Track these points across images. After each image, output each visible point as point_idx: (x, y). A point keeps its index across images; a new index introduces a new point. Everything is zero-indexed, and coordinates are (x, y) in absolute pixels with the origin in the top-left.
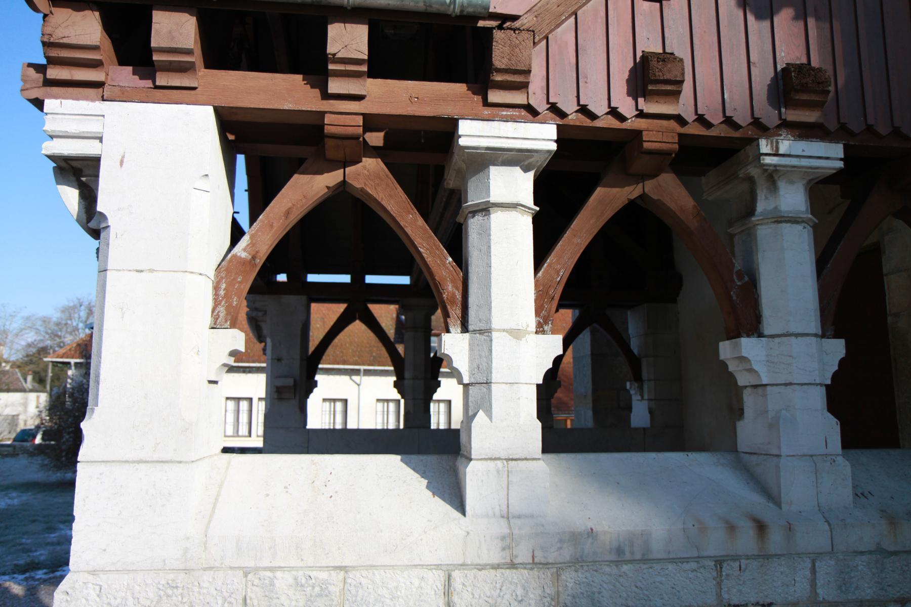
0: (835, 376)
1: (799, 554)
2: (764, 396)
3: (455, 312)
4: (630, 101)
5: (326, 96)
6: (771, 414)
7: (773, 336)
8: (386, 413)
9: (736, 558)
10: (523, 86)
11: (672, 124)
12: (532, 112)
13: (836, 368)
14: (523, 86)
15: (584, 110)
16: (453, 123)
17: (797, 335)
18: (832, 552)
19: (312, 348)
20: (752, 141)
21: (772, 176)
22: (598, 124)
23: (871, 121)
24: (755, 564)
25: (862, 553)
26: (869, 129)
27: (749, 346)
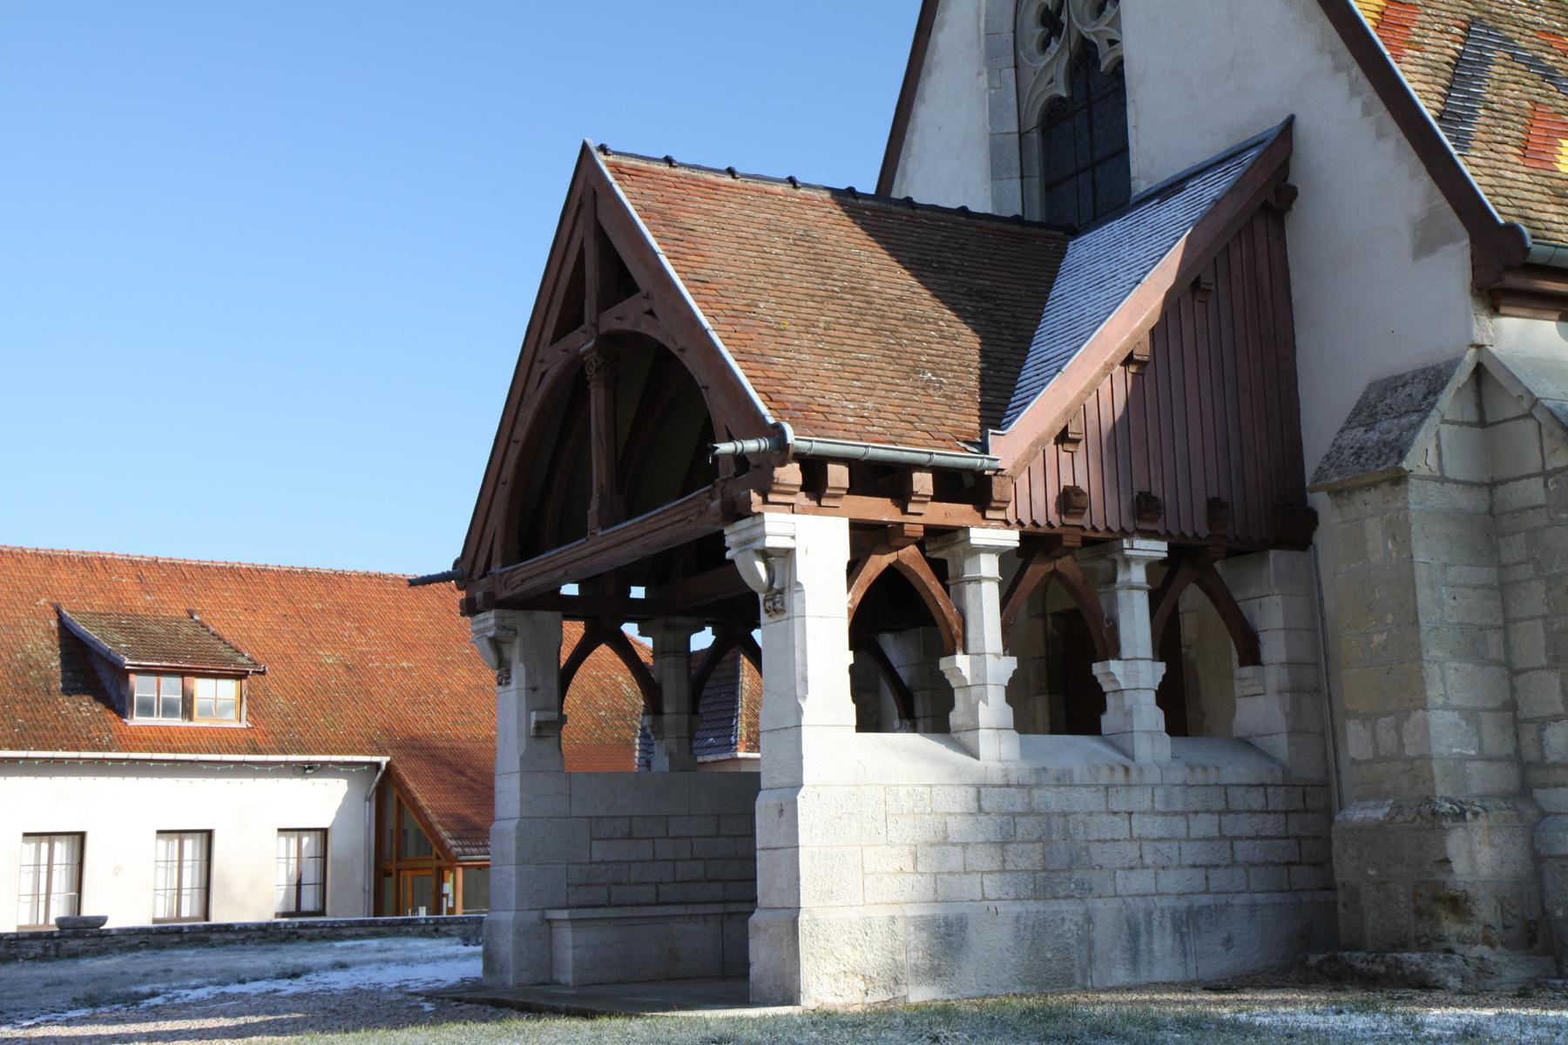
0: (1161, 685)
1: (1146, 785)
2: (1122, 696)
3: (959, 642)
4: (1057, 517)
5: (905, 511)
6: (1127, 707)
7: (1127, 660)
8: (44, 869)
9: (1115, 786)
10: (1004, 509)
11: (1078, 530)
12: (1007, 523)
13: (1160, 680)
14: (1004, 509)
15: (1034, 523)
16: (966, 529)
17: (1141, 659)
18: (1162, 784)
20: (1119, 540)
22: (1040, 530)
23: (1182, 529)
24: (1124, 789)
25: (1177, 785)
26: (1182, 533)
27: (1114, 666)
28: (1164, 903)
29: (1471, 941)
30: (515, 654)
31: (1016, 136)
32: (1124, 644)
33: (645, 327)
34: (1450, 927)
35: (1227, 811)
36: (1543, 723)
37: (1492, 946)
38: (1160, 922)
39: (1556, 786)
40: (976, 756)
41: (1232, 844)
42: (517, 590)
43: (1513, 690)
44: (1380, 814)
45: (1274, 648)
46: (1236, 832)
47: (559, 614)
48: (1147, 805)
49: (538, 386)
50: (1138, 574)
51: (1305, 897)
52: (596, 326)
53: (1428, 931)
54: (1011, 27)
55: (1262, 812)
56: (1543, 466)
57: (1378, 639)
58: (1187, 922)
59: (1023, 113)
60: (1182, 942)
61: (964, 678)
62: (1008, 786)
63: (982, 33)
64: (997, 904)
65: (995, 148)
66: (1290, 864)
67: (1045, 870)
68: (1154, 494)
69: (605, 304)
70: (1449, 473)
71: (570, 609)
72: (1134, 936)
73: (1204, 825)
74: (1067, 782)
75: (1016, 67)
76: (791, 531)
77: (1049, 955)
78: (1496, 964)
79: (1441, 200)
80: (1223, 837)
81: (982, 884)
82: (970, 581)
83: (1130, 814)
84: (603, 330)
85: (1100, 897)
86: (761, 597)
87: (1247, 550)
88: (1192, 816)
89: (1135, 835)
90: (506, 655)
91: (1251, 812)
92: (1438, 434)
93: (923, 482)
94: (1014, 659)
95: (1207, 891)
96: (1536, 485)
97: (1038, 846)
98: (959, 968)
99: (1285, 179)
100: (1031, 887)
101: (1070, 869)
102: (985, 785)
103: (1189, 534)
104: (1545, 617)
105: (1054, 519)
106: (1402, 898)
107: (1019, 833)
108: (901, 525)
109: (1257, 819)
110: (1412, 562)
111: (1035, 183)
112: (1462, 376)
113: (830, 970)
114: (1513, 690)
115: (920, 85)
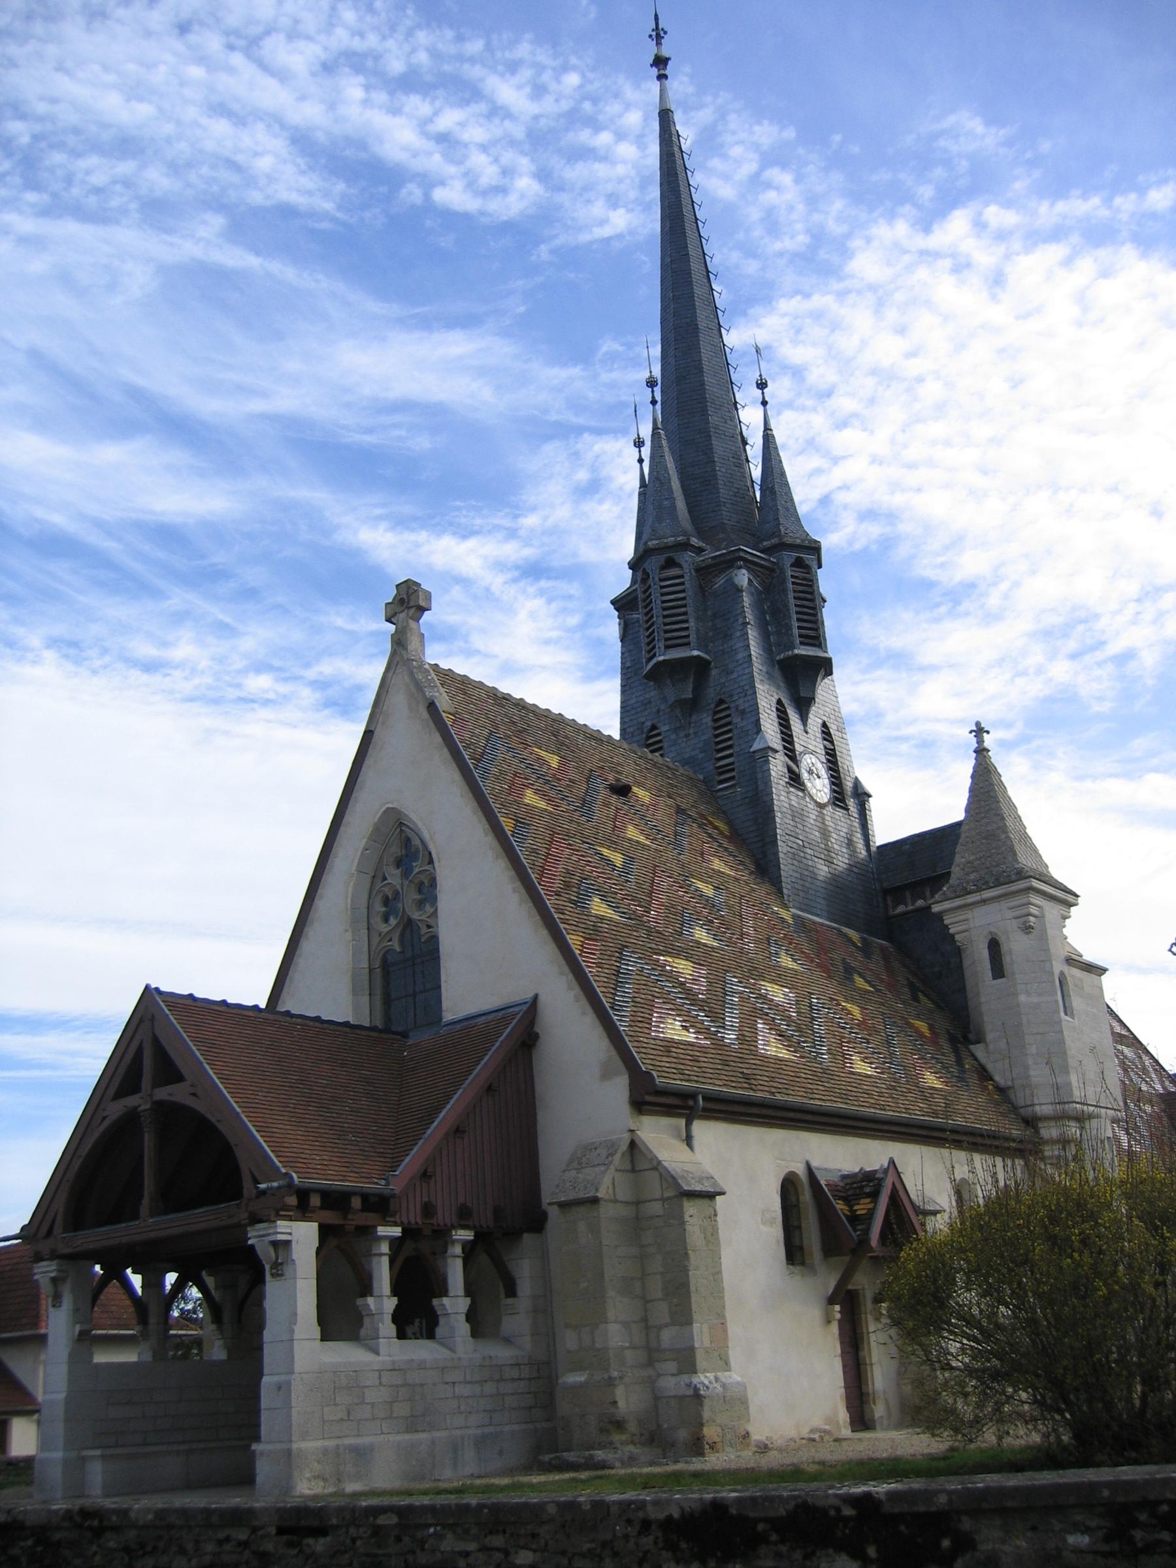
5: (345, 1218)
20: (451, 1231)
27: (445, 1300)
28: (470, 1432)
29: (626, 1443)
31: (368, 970)
33: (190, 1102)
34: (617, 1437)
35: (501, 1380)
36: (659, 1328)
39: (665, 1361)
40: (377, 1353)
42: (78, 1249)
44: (582, 1379)
45: (525, 1287)
49: (100, 1124)
51: (538, 1425)
52: (151, 1095)
54: (366, 906)
55: (518, 1379)
56: (662, 1195)
57: (584, 1285)
58: (481, 1442)
59: (372, 957)
61: (371, 1310)
62: (395, 1370)
63: (349, 907)
66: (531, 1408)
68: (469, 1204)
73: (489, 1388)
75: (368, 929)
77: (414, 1463)
79: (614, 1053)
82: (376, 1255)
85: (439, 1430)
86: (267, 1267)
87: (513, 1235)
91: (513, 1380)
92: (613, 1179)
93: (356, 1203)
95: (490, 1425)
99: (533, 1028)
102: (383, 1370)
103: (485, 1226)
105: (419, 1221)
108: (343, 1225)
112: (624, 1146)
113: (308, 1475)
114: (646, 1310)
115: (305, 929)
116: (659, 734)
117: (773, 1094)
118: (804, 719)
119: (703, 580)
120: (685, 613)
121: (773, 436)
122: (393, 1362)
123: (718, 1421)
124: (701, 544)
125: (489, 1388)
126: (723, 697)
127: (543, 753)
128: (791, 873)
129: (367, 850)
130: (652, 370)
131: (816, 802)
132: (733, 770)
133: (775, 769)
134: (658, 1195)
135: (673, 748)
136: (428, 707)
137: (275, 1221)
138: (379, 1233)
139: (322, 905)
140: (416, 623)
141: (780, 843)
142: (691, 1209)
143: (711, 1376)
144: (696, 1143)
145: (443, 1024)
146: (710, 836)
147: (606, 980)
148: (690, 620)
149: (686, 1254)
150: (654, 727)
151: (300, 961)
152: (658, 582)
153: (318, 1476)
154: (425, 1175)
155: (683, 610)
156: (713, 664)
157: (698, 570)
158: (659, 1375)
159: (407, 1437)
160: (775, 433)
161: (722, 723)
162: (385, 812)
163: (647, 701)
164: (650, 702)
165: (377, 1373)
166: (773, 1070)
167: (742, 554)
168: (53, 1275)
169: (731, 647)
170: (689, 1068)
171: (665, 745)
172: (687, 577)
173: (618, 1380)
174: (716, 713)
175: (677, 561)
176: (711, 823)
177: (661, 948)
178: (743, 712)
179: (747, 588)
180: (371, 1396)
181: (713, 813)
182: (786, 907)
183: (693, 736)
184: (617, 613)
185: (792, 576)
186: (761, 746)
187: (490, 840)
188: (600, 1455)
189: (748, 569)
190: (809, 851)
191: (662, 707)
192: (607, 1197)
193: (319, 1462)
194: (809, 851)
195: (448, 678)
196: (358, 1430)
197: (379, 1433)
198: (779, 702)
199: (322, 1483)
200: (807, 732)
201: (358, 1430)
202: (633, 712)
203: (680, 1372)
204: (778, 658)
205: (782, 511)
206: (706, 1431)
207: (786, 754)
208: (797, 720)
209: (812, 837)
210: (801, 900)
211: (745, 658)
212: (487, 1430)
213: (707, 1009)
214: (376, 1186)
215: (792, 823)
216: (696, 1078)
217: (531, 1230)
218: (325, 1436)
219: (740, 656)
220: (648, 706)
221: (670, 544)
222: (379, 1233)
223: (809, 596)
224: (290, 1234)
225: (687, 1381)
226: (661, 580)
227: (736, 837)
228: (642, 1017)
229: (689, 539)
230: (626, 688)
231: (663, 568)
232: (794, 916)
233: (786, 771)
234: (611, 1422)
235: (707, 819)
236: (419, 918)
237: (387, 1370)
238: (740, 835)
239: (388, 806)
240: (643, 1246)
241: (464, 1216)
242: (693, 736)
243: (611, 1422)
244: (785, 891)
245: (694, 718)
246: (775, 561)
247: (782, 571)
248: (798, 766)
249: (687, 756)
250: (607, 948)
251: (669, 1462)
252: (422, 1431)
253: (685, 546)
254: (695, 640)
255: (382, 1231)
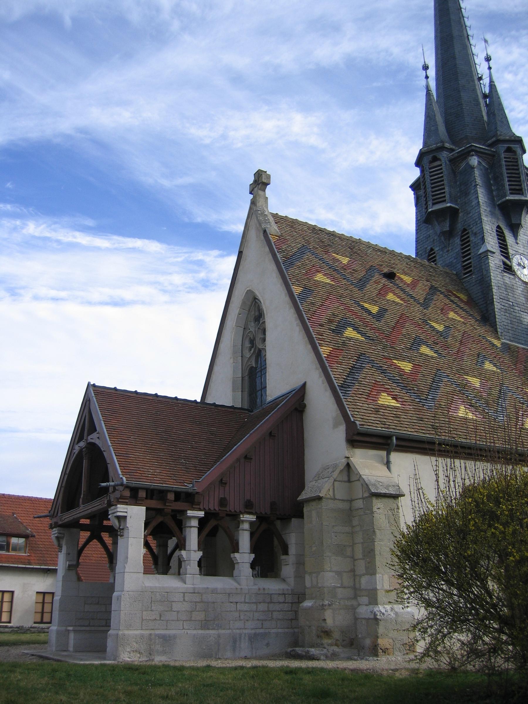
5: (165, 505)
10: (199, 505)
19: (80, 546)
21: (243, 521)
22: (212, 512)
27: (236, 555)
29: (331, 645)
30: (64, 543)
32: (240, 548)
34: (326, 641)
35: (271, 602)
36: (360, 576)
37: (338, 646)
38: (244, 638)
39: (363, 596)
41: (272, 613)
42: (63, 522)
43: (354, 566)
45: (292, 550)
46: (274, 609)
47: (79, 530)
48: (243, 600)
50: (246, 526)
52: (87, 440)
53: (319, 642)
55: (283, 603)
57: (314, 549)
58: (253, 638)
60: (251, 644)
64: (188, 631)
65: (234, 382)
66: (292, 619)
67: (205, 620)
68: (252, 500)
69: (90, 433)
70: (337, 497)
71: (84, 528)
72: (235, 641)
73: (262, 607)
74: (215, 592)
75: (242, 356)
76: (126, 511)
77: (204, 648)
78: (338, 652)
80: (269, 611)
81: (183, 624)
83: (237, 603)
84: (88, 441)
85: (224, 629)
87: (286, 519)
88: (258, 604)
89: (238, 610)
90: (61, 543)
91: (280, 603)
93: (171, 496)
94: (202, 552)
95: (262, 628)
96: (361, 501)
97: (204, 613)
98: (173, 651)
99: (303, 401)
100: (200, 625)
101: (214, 620)
102: (186, 593)
104: (362, 543)
106: (314, 631)
107: (197, 608)
109: (281, 605)
110: (322, 525)
111: (246, 394)
112: (342, 467)
113: (128, 650)
116: (434, 253)
117: (454, 438)
118: (515, 236)
119: (454, 166)
120: (443, 185)
121: (495, 85)
122: (194, 588)
123: (390, 635)
124: (452, 147)
125: (262, 607)
126: (465, 227)
127: (338, 257)
128: (504, 320)
129: (240, 314)
130: (426, 61)
131: (523, 281)
132: (471, 267)
133: (493, 262)
134: (361, 496)
135: (441, 259)
136: (264, 233)
137: (116, 505)
138: (188, 515)
139: (222, 346)
140: (263, 192)
141: (495, 303)
142: (378, 505)
143: (388, 607)
144: (392, 466)
145: (267, 403)
146: (452, 301)
147: (342, 371)
148: (446, 188)
149: (374, 531)
150: (432, 249)
151: (214, 377)
152: (428, 170)
153: (136, 651)
154: (222, 482)
155: (442, 183)
156: (460, 210)
157: (450, 161)
158: (359, 605)
159: (200, 632)
160: (496, 84)
161: (465, 242)
162: (246, 293)
163: (428, 236)
164: (430, 236)
165: (182, 594)
166: (458, 425)
167: (473, 148)
168: (56, 535)
169: (469, 199)
170: (390, 421)
171: (437, 258)
172: (443, 165)
173: (327, 607)
174: (462, 236)
175: (438, 157)
176: (455, 295)
177: (392, 356)
178: (475, 234)
179: (477, 166)
180: (176, 607)
181: (458, 291)
182: (498, 339)
183: (451, 251)
184: (413, 192)
185: (505, 158)
186: (484, 250)
187: (287, 299)
188: (313, 651)
189: (479, 157)
190: (517, 308)
191: (436, 238)
192: (328, 496)
193: (137, 643)
194: (517, 308)
195: (279, 219)
196: (167, 626)
197: (182, 628)
198: (498, 227)
199: (139, 655)
200: (517, 243)
201: (167, 626)
202: (421, 243)
203: (370, 604)
204: (498, 203)
205: (499, 123)
206: (380, 641)
207: (502, 255)
208: (511, 237)
209: (519, 300)
210: (511, 335)
211: (476, 204)
212: (258, 631)
213: (416, 389)
214: (188, 487)
215: (505, 293)
216: (394, 427)
217: (295, 516)
218: (143, 628)
219: (473, 203)
220: (429, 239)
221: (434, 148)
222: (188, 515)
223: (515, 168)
224: (126, 512)
225: (371, 609)
226: (430, 169)
227: (471, 302)
228: (363, 392)
229: (443, 144)
230: (418, 231)
231: (431, 162)
232: (503, 344)
233: (502, 264)
234: (322, 632)
235: (452, 293)
236: (262, 347)
237: (190, 593)
238: (475, 302)
239: (248, 289)
240: (354, 527)
241: (249, 507)
242: (451, 251)
243: (322, 632)
244: (499, 330)
245: (451, 242)
246: (495, 150)
247: (499, 156)
248: (510, 262)
249: (447, 262)
250: (349, 354)
251: (358, 659)
252: (212, 629)
253: (442, 148)
254: (448, 198)
255: (190, 513)
